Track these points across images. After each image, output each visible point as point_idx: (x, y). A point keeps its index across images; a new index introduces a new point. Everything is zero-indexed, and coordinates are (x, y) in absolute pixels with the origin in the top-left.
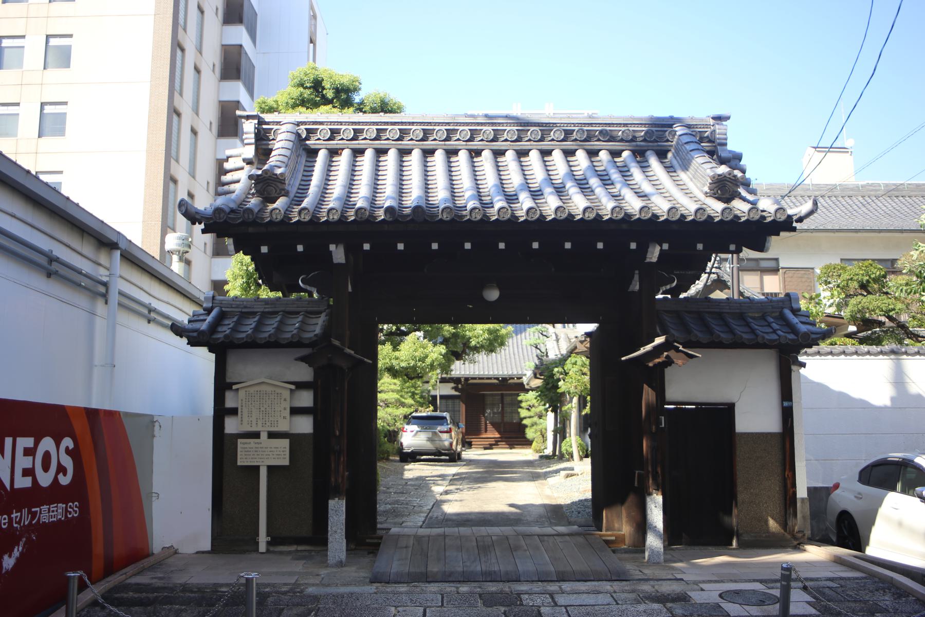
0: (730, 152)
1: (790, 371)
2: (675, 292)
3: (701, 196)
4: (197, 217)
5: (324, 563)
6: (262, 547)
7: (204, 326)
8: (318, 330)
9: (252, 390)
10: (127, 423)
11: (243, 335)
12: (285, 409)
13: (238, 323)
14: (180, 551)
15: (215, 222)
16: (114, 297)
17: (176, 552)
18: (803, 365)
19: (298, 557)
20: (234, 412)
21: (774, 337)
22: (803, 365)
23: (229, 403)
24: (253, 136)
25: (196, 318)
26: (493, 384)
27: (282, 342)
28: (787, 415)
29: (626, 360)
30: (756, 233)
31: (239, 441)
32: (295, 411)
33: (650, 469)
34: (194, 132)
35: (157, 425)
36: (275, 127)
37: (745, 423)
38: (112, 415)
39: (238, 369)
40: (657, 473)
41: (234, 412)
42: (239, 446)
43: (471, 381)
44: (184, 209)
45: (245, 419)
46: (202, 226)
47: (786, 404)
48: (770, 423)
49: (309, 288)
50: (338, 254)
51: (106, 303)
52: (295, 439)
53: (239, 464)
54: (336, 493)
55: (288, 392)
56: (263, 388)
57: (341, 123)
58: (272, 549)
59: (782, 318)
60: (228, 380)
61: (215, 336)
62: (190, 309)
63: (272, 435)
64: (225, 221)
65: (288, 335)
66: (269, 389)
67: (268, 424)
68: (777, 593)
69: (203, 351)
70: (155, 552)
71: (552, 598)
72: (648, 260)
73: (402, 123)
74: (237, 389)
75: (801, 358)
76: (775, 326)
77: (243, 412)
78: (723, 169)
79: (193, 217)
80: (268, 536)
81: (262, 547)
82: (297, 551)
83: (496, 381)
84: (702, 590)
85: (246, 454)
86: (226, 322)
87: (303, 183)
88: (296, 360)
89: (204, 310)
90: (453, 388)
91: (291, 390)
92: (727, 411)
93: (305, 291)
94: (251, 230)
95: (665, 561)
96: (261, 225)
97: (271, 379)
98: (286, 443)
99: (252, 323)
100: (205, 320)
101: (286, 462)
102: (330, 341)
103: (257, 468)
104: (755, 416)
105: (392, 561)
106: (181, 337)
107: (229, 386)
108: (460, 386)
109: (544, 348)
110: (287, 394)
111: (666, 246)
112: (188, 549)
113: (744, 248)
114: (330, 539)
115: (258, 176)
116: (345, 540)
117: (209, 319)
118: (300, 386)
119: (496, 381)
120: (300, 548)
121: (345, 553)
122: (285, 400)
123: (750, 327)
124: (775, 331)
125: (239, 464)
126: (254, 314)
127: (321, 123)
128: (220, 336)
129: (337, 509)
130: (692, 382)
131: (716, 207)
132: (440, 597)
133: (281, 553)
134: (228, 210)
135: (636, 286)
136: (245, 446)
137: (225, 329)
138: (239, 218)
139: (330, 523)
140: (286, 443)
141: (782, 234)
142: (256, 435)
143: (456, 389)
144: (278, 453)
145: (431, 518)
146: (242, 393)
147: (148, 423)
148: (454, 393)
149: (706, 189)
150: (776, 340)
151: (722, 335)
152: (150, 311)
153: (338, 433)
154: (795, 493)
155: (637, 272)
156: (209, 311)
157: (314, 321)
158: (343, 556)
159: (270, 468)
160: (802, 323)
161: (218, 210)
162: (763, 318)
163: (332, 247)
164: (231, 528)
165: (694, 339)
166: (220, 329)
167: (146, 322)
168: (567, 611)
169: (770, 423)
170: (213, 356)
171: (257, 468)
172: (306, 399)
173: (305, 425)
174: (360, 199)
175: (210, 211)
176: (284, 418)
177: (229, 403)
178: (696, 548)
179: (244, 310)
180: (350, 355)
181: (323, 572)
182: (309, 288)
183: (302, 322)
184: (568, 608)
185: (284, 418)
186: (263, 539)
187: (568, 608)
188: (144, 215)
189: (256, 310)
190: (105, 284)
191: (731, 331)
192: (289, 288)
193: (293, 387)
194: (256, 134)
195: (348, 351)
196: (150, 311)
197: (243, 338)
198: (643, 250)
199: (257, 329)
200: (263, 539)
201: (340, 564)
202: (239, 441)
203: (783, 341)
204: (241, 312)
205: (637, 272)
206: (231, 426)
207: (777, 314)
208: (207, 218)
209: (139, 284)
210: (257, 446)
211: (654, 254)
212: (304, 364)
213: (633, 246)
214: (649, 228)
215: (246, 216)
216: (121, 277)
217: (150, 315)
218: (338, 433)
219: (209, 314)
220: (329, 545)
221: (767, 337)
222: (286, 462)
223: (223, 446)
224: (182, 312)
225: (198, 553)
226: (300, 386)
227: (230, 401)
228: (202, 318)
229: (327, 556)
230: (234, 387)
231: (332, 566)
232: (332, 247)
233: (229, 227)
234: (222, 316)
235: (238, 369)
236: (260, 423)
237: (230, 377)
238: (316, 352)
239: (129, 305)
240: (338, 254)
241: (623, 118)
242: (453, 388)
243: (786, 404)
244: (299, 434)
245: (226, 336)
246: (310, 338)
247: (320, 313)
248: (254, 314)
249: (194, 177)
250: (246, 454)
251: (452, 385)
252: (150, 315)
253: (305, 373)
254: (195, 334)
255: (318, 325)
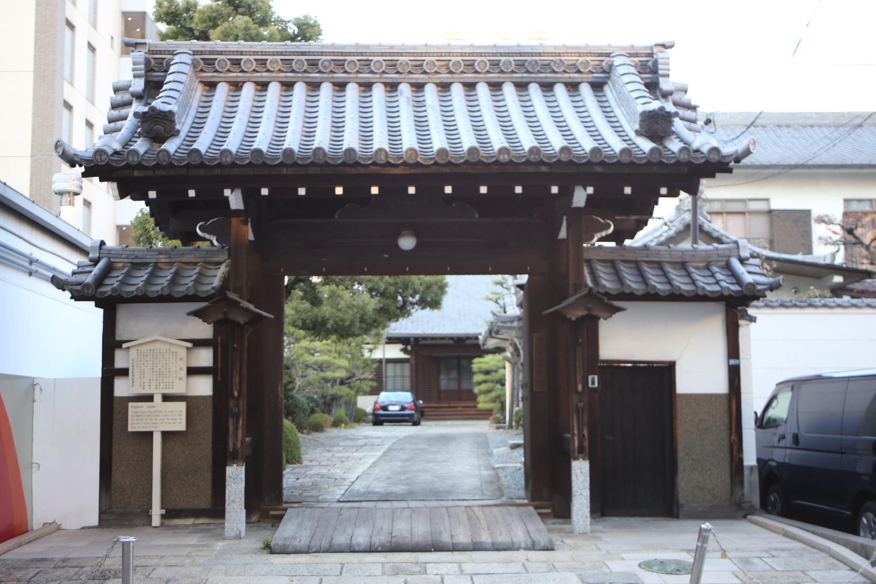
0: (674, 84)
3: (632, 135)
4: (76, 159)
6: (156, 521)
7: (89, 279)
8: (216, 282)
9: (144, 349)
11: (133, 288)
12: (181, 369)
14: (63, 527)
15: (96, 165)
17: (59, 528)
18: (752, 319)
19: (196, 530)
20: (124, 372)
21: (716, 288)
22: (752, 319)
23: (119, 364)
24: (142, 66)
25: (81, 270)
27: (176, 296)
28: (734, 374)
29: (551, 313)
30: (689, 173)
31: (130, 404)
32: (193, 371)
33: (576, 432)
37: (686, 383)
41: (124, 372)
42: (130, 410)
43: (422, 342)
44: (60, 150)
46: (83, 169)
47: (732, 362)
49: (207, 236)
50: (235, 199)
52: (192, 403)
53: (130, 429)
54: (234, 458)
55: (185, 351)
56: (157, 346)
57: (242, 53)
58: (166, 522)
59: (728, 267)
60: (118, 338)
62: (77, 258)
63: (166, 398)
64: (108, 164)
65: (183, 288)
66: (164, 347)
67: (162, 385)
68: (689, 558)
69: (90, 305)
70: (35, 528)
71: (460, 567)
74: (128, 348)
75: (751, 311)
76: (719, 276)
80: (162, 508)
81: (156, 521)
83: (451, 342)
84: (623, 559)
85: (138, 419)
86: (115, 274)
87: (197, 120)
88: (189, 314)
89: (91, 261)
90: (401, 350)
91: (188, 348)
92: (665, 372)
94: (136, 173)
95: (592, 532)
97: (165, 336)
98: (182, 406)
99: (143, 275)
100: (91, 272)
101: (182, 427)
102: (225, 294)
103: (150, 434)
104: (699, 373)
105: (290, 529)
106: (64, 290)
107: (119, 345)
109: (476, 303)
110: (183, 353)
112: (73, 524)
115: (144, 113)
116: (244, 511)
117: (96, 270)
118: (198, 343)
120: (198, 521)
121: (244, 525)
122: (181, 359)
124: (717, 282)
125: (130, 429)
127: (221, 53)
129: (236, 477)
130: (624, 340)
131: (646, 145)
132: (339, 566)
134: (110, 152)
135: (563, 234)
136: (137, 410)
137: (113, 283)
138: (123, 161)
140: (182, 406)
141: (718, 175)
142: (149, 398)
143: (405, 351)
144: (175, 418)
145: (352, 491)
146: (133, 352)
147: (31, 384)
148: (402, 355)
149: (637, 127)
150: (717, 292)
152: (31, 262)
153: (236, 394)
154: (741, 460)
155: (565, 218)
156: (95, 262)
157: (212, 273)
158: (242, 526)
159: (165, 435)
160: (749, 272)
161: (99, 152)
162: (707, 267)
163: (227, 192)
164: (120, 503)
165: (627, 291)
166: (107, 281)
168: (472, 579)
170: (101, 311)
171: (150, 434)
172: (205, 358)
173: (204, 387)
175: (90, 154)
176: (180, 379)
179: (135, 261)
182: (207, 236)
183: (200, 274)
184: (474, 577)
185: (180, 379)
186: (157, 511)
187: (474, 577)
188: (33, 147)
189: (147, 261)
191: (645, 280)
192: (189, 238)
193: (190, 345)
195: (245, 304)
196: (31, 263)
197: (133, 292)
198: (567, 193)
200: (157, 511)
201: (238, 537)
202: (130, 404)
203: (726, 293)
204: (132, 263)
205: (565, 218)
207: (723, 263)
208: (86, 160)
210: (150, 409)
211: (580, 197)
212: (197, 319)
213: (555, 190)
214: (570, 169)
215: (131, 159)
218: (236, 394)
221: (708, 288)
222: (182, 427)
223: (112, 410)
224: (66, 263)
225: (83, 528)
226: (198, 343)
227: (120, 362)
228: (87, 269)
229: (224, 528)
230: (125, 345)
231: (230, 539)
232: (227, 192)
233: (115, 170)
234: (109, 269)
235: (125, 327)
236: (153, 385)
238: (211, 305)
240: (235, 199)
241: (555, 47)
242: (401, 350)
243: (732, 362)
245: (114, 290)
246: (208, 291)
247: (220, 263)
248: (145, 265)
249: (92, 103)
250: (138, 419)
251: (401, 346)
252: (31, 267)
253: (204, 330)
254: (79, 288)
255: (216, 277)
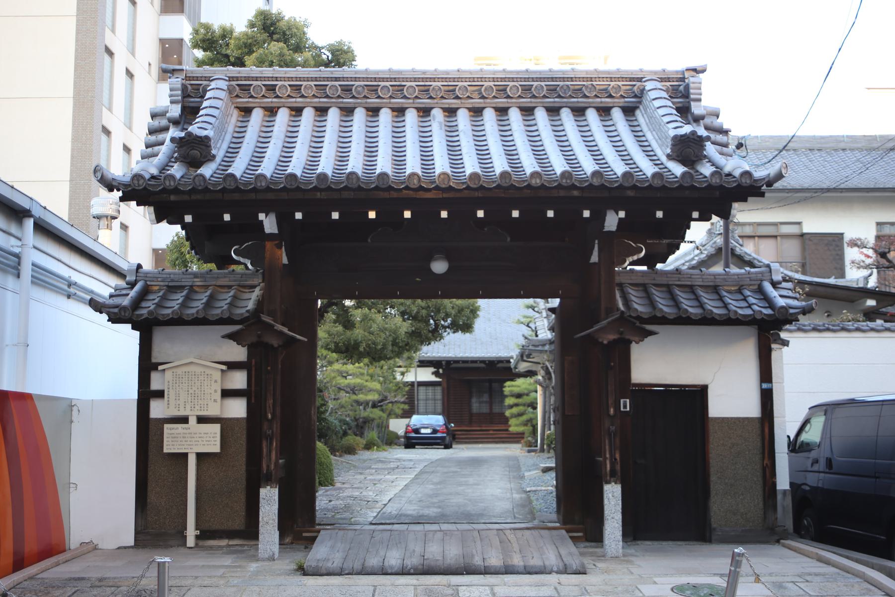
0: (705, 108)
1: (770, 350)
2: (650, 261)
3: (664, 159)
4: (114, 183)
5: (255, 558)
6: (191, 541)
7: (126, 302)
8: (251, 305)
9: (179, 371)
10: (39, 406)
11: (169, 311)
13: (164, 298)
14: (100, 547)
15: (134, 189)
16: (26, 270)
17: (95, 548)
18: (785, 343)
19: (230, 550)
20: (160, 394)
21: (749, 312)
22: (785, 343)
23: (155, 385)
25: (118, 292)
26: (478, 368)
28: (767, 398)
30: (721, 197)
31: (166, 426)
32: (227, 394)
33: (608, 456)
34: (130, 74)
35: (75, 409)
36: (205, 83)
37: (717, 408)
38: (24, 398)
39: (165, 345)
40: (616, 459)
41: (160, 394)
45: (172, 402)
46: (120, 194)
47: (765, 386)
48: (747, 406)
49: (242, 260)
50: (269, 223)
51: (19, 277)
53: (165, 451)
54: (268, 480)
55: (219, 373)
57: (276, 79)
58: (201, 543)
59: (760, 290)
60: (154, 360)
61: (137, 313)
62: (114, 281)
63: (201, 420)
64: (145, 188)
65: (218, 311)
66: (198, 370)
67: (197, 407)
69: (126, 328)
72: (606, 229)
73: (347, 79)
75: (783, 335)
76: (751, 300)
77: (170, 394)
78: (687, 129)
79: (110, 185)
81: (191, 541)
82: (229, 546)
83: (483, 365)
84: (655, 583)
86: (151, 297)
88: (223, 337)
90: (433, 373)
91: (222, 371)
92: (699, 394)
93: (239, 263)
94: (172, 198)
95: (624, 556)
96: (183, 192)
97: (200, 358)
98: (216, 428)
99: (179, 297)
100: (127, 295)
101: (217, 449)
102: (260, 317)
103: (185, 456)
104: (731, 396)
105: (322, 551)
106: (101, 313)
107: (155, 367)
108: (441, 371)
109: (506, 326)
111: (622, 214)
112: (109, 544)
113: (713, 216)
114: (261, 530)
115: (181, 138)
116: (278, 533)
117: (133, 293)
118: (233, 366)
119: (483, 365)
120: (232, 542)
121: (278, 546)
122: (216, 381)
123: (723, 302)
124: (750, 306)
125: (165, 451)
126: (182, 288)
128: (144, 312)
129: (269, 499)
130: (655, 364)
132: (372, 588)
133: (211, 548)
134: (147, 176)
136: (173, 431)
137: (149, 305)
138: (160, 185)
139: (261, 513)
140: (216, 428)
142: (184, 420)
143: (436, 374)
144: (209, 440)
145: (384, 513)
146: (168, 374)
147: (69, 406)
148: (434, 378)
149: (669, 151)
150: (750, 315)
151: (690, 310)
154: (774, 484)
155: (597, 242)
156: (132, 285)
157: (246, 296)
158: (276, 548)
159: (200, 456)
160: (781, 296)
161: (137, 177)
162: (739, 291)
163: (262, 216)
164: (155, 524)
166: (144, 304)
167: (65, 299)
169: (747, 406)
171: (185, 456)
172: (239, 380)
173: (238, 409)
174: (267, 168)
175: (127, 179)
176: (215, 401)
177: (155, 385)
178: (664, 543)
179: (170, 284)
180: (281, 333)
181: (253, 566)
182: (242, 260)
183: (235, 297)
185: (215, 401)
186: (191, 532)
189: (183, 284)
190: (18, 256)
191: (677, 304)
192: (224, 261)
193: (224, 367)
194: (183, 91)
196: (69, 286)
197: (168, 315)
198: (599, 217)
199: (184, 305)
200: (191, 532)
201: (272, 559)
202: (166, 426)
203: (758, 317)
204: (168, 286)
206: (157, 409)
207: (756, 287)
209: (57, 256)
210: (185, 431)
211: (612, 221)
214: (602, 193)
215: (167, 183)
216: (35, 247)
217: (70, 290)
219: (132, 288)
220: (260, 537)
221: (740, 312)
222: (217, 449)
223: (148, 431)
224: (103, 286)
225: (119, 548)
226: (233, 366)
227: (156, 384)
228: (124, 292)
229: (257, 549)
230: (160, 368)
231: (263, 560)
232: (262, 216)
235: (162, 348)
236: (188, 407)
237: (156, 357)
239: (43, 279)
240: (269, 223)
243: (765, 386)
244: (234, 419)
245: (150, 313)
246: (242, 314)
247: (254, 287)
249: (130, 128)
250: (173, 440)
251: (432, 369)
253: (239, 353)
254: (116, 310)
